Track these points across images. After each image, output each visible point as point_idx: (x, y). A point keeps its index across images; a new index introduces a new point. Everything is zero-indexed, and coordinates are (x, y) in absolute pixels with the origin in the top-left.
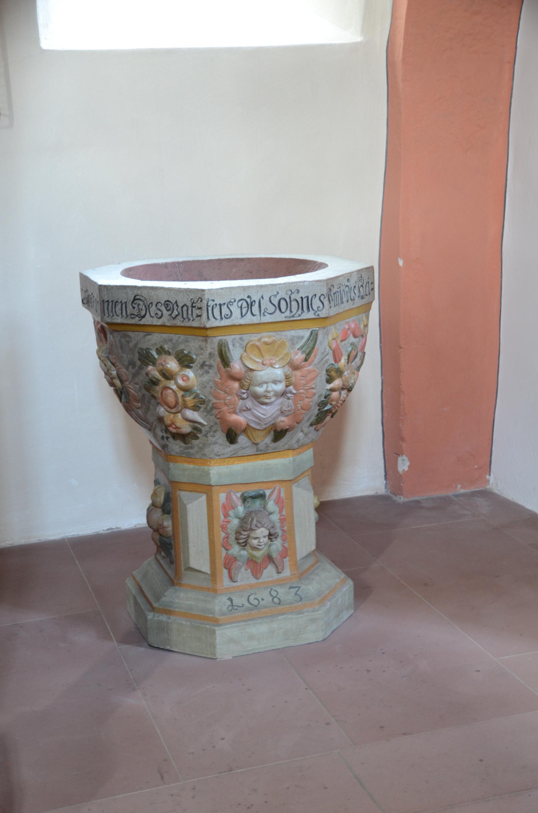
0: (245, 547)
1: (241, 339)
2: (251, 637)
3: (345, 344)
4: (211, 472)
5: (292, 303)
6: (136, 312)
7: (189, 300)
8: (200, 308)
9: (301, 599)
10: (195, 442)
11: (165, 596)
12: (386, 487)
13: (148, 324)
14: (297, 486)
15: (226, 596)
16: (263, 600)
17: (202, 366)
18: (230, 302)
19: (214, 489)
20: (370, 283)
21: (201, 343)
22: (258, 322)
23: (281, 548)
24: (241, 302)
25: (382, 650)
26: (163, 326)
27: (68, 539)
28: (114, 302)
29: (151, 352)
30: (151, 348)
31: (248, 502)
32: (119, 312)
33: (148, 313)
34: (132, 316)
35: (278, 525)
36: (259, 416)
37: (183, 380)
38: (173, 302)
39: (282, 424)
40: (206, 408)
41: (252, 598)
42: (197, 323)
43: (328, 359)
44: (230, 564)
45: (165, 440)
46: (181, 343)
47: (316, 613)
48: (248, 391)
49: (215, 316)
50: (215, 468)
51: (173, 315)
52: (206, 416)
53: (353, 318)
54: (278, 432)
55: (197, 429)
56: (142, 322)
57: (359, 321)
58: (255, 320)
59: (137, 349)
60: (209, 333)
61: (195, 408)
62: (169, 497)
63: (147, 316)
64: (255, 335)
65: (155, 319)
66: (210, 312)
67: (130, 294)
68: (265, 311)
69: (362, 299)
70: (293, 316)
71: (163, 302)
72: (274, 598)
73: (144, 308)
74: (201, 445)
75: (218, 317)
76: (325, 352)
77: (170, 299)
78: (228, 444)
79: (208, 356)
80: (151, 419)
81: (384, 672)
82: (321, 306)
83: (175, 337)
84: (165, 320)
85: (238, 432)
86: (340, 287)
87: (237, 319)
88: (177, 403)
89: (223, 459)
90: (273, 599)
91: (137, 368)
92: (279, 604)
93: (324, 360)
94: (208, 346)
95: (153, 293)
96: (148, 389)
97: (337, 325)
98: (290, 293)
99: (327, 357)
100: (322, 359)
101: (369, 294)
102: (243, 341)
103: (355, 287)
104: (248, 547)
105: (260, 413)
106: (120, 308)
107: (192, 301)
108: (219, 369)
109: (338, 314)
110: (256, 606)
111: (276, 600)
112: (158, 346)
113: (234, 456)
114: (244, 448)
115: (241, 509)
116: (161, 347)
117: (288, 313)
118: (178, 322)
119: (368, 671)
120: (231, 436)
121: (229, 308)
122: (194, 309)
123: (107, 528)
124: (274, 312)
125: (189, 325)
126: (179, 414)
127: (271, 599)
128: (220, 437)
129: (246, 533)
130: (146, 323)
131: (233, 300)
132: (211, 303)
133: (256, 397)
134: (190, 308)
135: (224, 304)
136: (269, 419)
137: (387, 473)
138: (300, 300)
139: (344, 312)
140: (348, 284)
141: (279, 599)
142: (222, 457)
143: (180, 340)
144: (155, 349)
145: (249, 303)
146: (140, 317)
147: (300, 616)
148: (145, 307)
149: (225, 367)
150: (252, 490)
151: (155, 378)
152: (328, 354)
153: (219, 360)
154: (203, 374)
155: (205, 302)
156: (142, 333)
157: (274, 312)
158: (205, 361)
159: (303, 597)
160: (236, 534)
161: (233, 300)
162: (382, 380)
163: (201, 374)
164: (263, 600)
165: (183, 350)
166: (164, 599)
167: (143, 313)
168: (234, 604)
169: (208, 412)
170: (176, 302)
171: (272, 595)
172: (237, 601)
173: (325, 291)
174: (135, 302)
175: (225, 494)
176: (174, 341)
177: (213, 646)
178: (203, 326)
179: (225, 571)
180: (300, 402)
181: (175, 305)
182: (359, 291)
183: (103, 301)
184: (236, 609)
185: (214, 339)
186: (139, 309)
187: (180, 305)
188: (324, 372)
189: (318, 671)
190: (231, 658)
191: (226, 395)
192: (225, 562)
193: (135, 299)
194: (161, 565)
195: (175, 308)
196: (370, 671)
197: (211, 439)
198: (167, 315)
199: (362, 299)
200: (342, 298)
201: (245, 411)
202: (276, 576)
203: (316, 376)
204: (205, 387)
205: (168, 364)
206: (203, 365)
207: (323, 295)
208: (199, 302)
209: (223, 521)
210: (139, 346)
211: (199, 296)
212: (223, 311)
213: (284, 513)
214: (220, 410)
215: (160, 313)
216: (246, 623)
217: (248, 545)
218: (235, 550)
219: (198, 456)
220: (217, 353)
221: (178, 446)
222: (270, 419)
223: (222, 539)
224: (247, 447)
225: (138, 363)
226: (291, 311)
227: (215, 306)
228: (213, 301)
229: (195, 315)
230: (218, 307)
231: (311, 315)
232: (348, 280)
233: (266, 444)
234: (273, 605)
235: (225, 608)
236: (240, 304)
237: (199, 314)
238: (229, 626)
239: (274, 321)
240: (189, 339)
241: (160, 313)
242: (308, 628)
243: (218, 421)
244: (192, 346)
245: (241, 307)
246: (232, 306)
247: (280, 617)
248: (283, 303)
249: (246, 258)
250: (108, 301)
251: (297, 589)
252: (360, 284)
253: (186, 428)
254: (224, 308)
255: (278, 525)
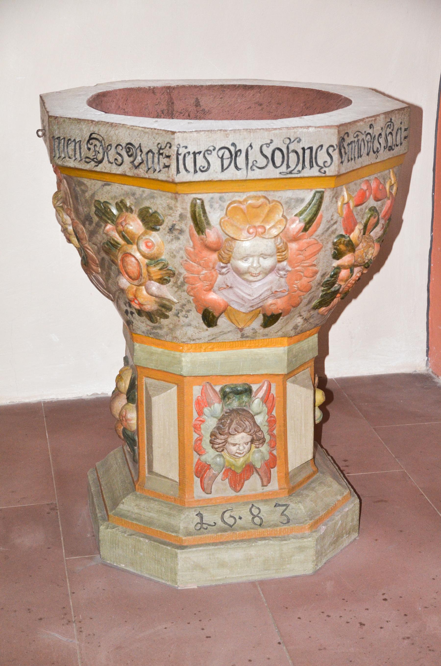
0: (222, 453)
1: (221, 198)
2: (222, 565)
3: (361, 210)
4: (183, 359)
5: (290, 155)
6: (91, 154)
7: (156, 144)
8: (168, 157)
9: (288, 522)
10: (164, 322)
11: (123, 503)
12: (427, 365)
13: (106, 171)
14: (294, 382)
15: (195, 511)
16: (240, 518)
17: (170, 230)
18: (207, 150)
19: (186, 380)
20: (403, 130)
21: (169, 201)
22: (244, 178)
23: (267, 457)
24: (223, 151)
25: (384, 594)
26: (124, 175)
27: (45, 403)
28: (66, 140)
29: (110, 206)
30: (110, 201)
31: (229, 398)
32: (71, 153)
33: (106, 158)
34: (87, 160)
35: (265, 429)
36: (243, 297)
37: (147, 246)
38: (137, 146)
39: (273, 308)
40: (176, 283)
41: (227, 515)
42: (164, 175)
43: (336, 229)
44: (203, 473)
45: (129, 315)
46: (145, 198)
47: (305, 540)
48: (229, 265)
49: (188, 168)
50: (189, 354)
51: (135, 162)
52: (176, 292)
53: (375, 176)
54: (268, 317)
55: (164, 308)
56: (98, 169)
57: (384, 179)
58: (240, 175)
59: (94, 201)
60: (179, 188)
61: (163, 281)
62: (135, 383)
63: (104, 161)
64: (239, 194)
65: (114, 166)
66: (181, 162)
67: (85, 130)
68: (253, 165)
69: (389, 150)
70: (291, 173)
71: (124, 145)
72: (254, 517)
73: (101, 151)
74: (171, 326)
75: (191, 169)
76: (332, 219)
77: (132, 142)
78: (205, 327)
79: (178, 218)
80: (114, 289)
81: (381, 628)
82: (329, 160)
83: (138, 191)
84: (126, 168)
85: (216, 314)
86: (357, 136)
87: (215, 173)
88: (140, 274)
89: (197, 345)
90: (253, 518)
91: (94, 225)
92: (260, 525)
93: (331, 230)
94: (178, 205)
95: (112, 133)
96: (107, 252)
97: (352, 185)
98: (288, 141)
99: (335, 227)
100: (328, 228)
101: (401, 144)
102: (224, 202)
103: (380, 134)
104: (224, 453)
105: (245, 293)
106: (73, 148)
107: (159, 146)
108: (191, 236)
109: (353, 170)
110: (231, 526)
111: (257, 520)
112: (119, 200)
113: (213, 344)
114: (225, 333)
115: (217, 407)
116: (122, 202)
117: (283, 168)
118: (141, 172)
119: (362, 624)
120: (209, 319)
121: (206, 159)
122: (161, 156)
123: (91, 393)
124: (266, 165)
125: (154, 178)
126: (143, 287)
127: (251, 517)
128: (196, 318)
129: (222, 437)
130: (103, 170)
131: (211, 148)
132: (182, 151)
133: (239, 273)
134: (156, 156)
135: (200, 153)
136: (256, 300)
137: (430, 348)
138: (300, 152)
139: (362, 167)
140: (370, 131)
141: (261, 519)
142: (198, 341)
143: (144, 195)
144: (114, 204)
145: (233, 153)
146: (96, 162)
147: (285, 542)
148: (103, 149)
149: (198, 234)
150: (239, 382)
151: (113, 240)
152: (336, 223)
153: (190, 223)
154: (172, 240)
155: (174, 148)
156: (99, 182)
157: (266, 165)
158: (175, 224)
159: (291, 518)
160: (211, 436)
161: (211, 148)
162: (432, 237)
163: (169, 239)
164: (240, 518)
165: (149, 208)
166: (121, 506)
167: (100, 157)
168: (204, 522)
169: (179, 287)
170: (140, 146)
171: (252, 514)
172: (208, 518)
173: (335, 141)
174: (91, 142)
175: (201, 387)
176: (137, 196)
177: (174, 571)
178: (171, 180)
179: (197, 480)
180: (296, 282)
181: (138, 151)
182: (387, 141)
183: (53, 137)
184: (206, 529)
185: (185, 197)
186: (95, 151)
187: (145, 150)
188: (330, 245)
189: (299, 618)
190: (196, 587)
191: (200, 268)
192: (197, 469)
193: (90, 138)
194: (126, 459)
195: (139, 153)
196: (364, 625)
197: (183, 320)
198: (129, 163)
199: (389, 150)
200: (359, 149)
201: (225, 288)
202: (260, 489)
203: (319, 251)
204: (175, 256)
205: (129, 224)
206: (172, 229)
207: (332, 146)
208: (167, 148)
209: (196, 420)
210: (96, 198)
211: (168, 140)
212: (198, 161)
213: (274, 413)
214: (194, 286)
215: (119, 159)
216: (216, 547)
217: (225, 451)
218: (210, 455)
219: (169, 338)
220: (189, 215)
221: (144, 324)
222: (257, 301)
223: (194, 441)
224: (229, 332)
225: (96, 219)
226: (288, 167)
227: (187, 155)
228: (186, 147)
229: (162, 165)
230: (192, 156)
231: (315, 172)
232: (371, 126)
233: (253, 329)
234: (253, 526)
235: (192, 527)
236: (220, 154)
237: (167, 164)
238: (194, 549)
239: (265, 177)
240: (156, 195)
241: (119, 159)
242: (295, 558)
243: (191, 298)
244: (159, 203)
245: (222, 158)
246: (210, 156)
247: (260, 543)
248: (278, 154)
249: (256, 86)
250: (58, 138)
251: (284, 507)
252: (389, 130)
253: (150, 305)
254: (200, 158)
255: (265, 429)
